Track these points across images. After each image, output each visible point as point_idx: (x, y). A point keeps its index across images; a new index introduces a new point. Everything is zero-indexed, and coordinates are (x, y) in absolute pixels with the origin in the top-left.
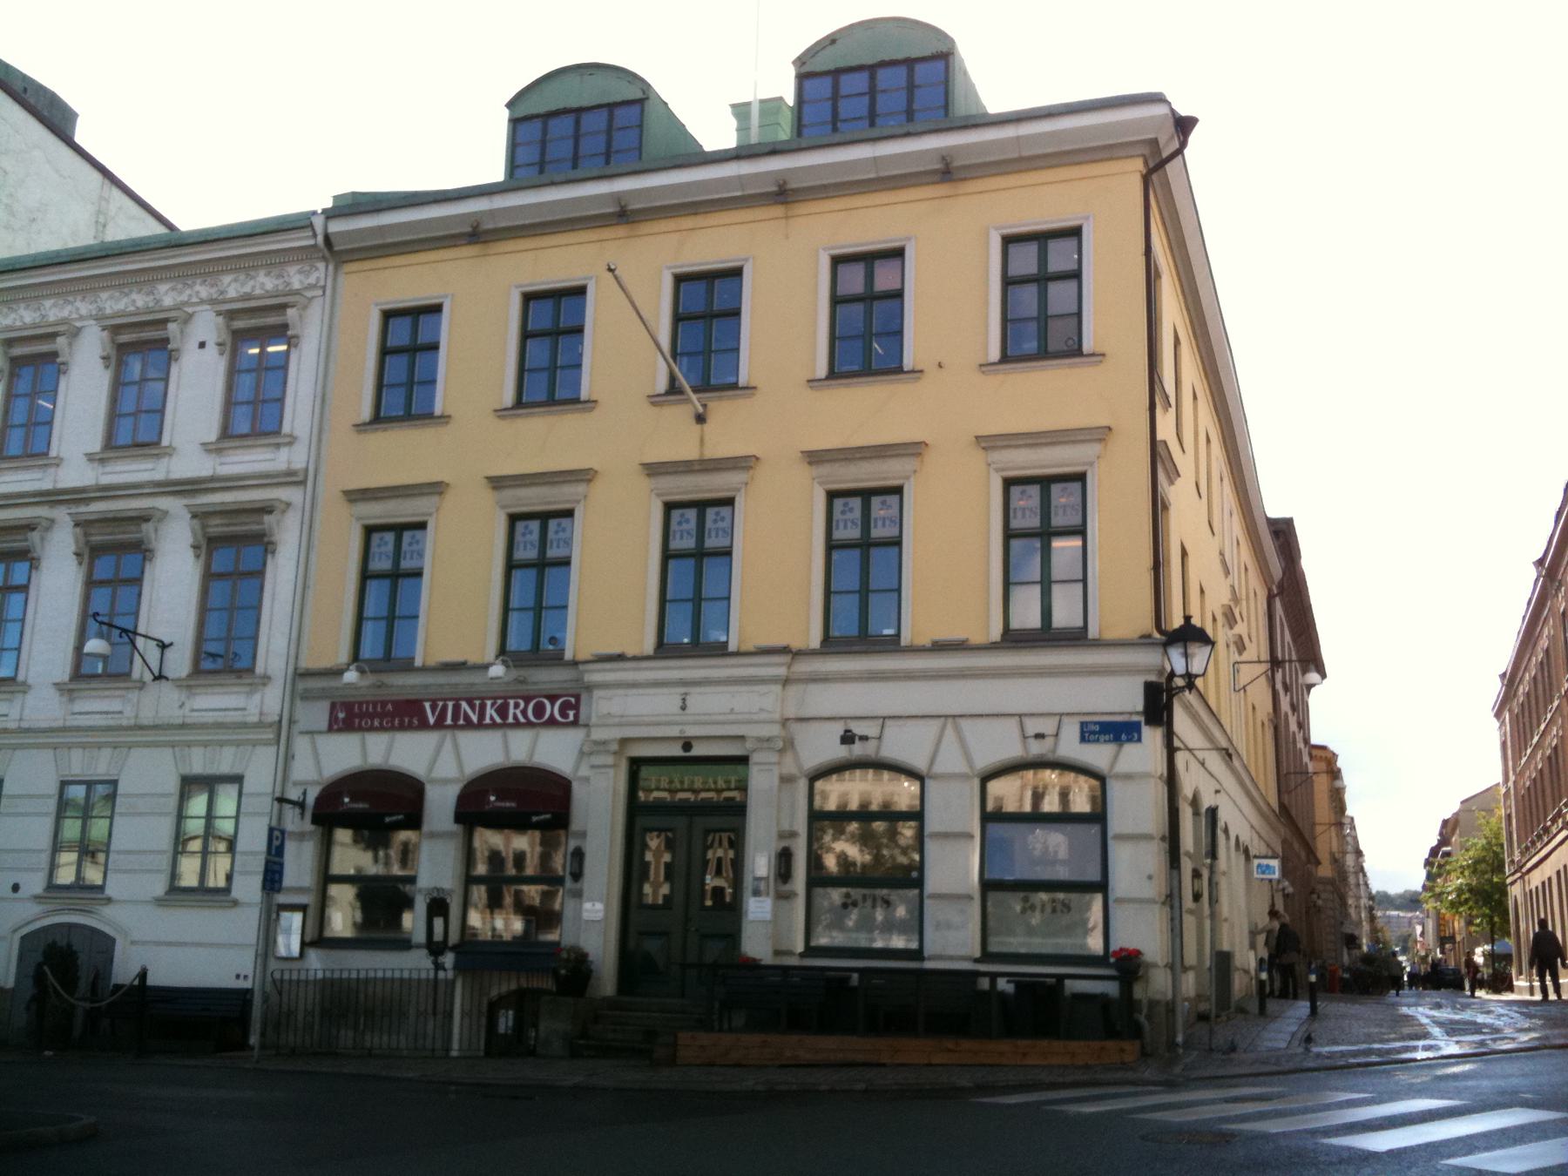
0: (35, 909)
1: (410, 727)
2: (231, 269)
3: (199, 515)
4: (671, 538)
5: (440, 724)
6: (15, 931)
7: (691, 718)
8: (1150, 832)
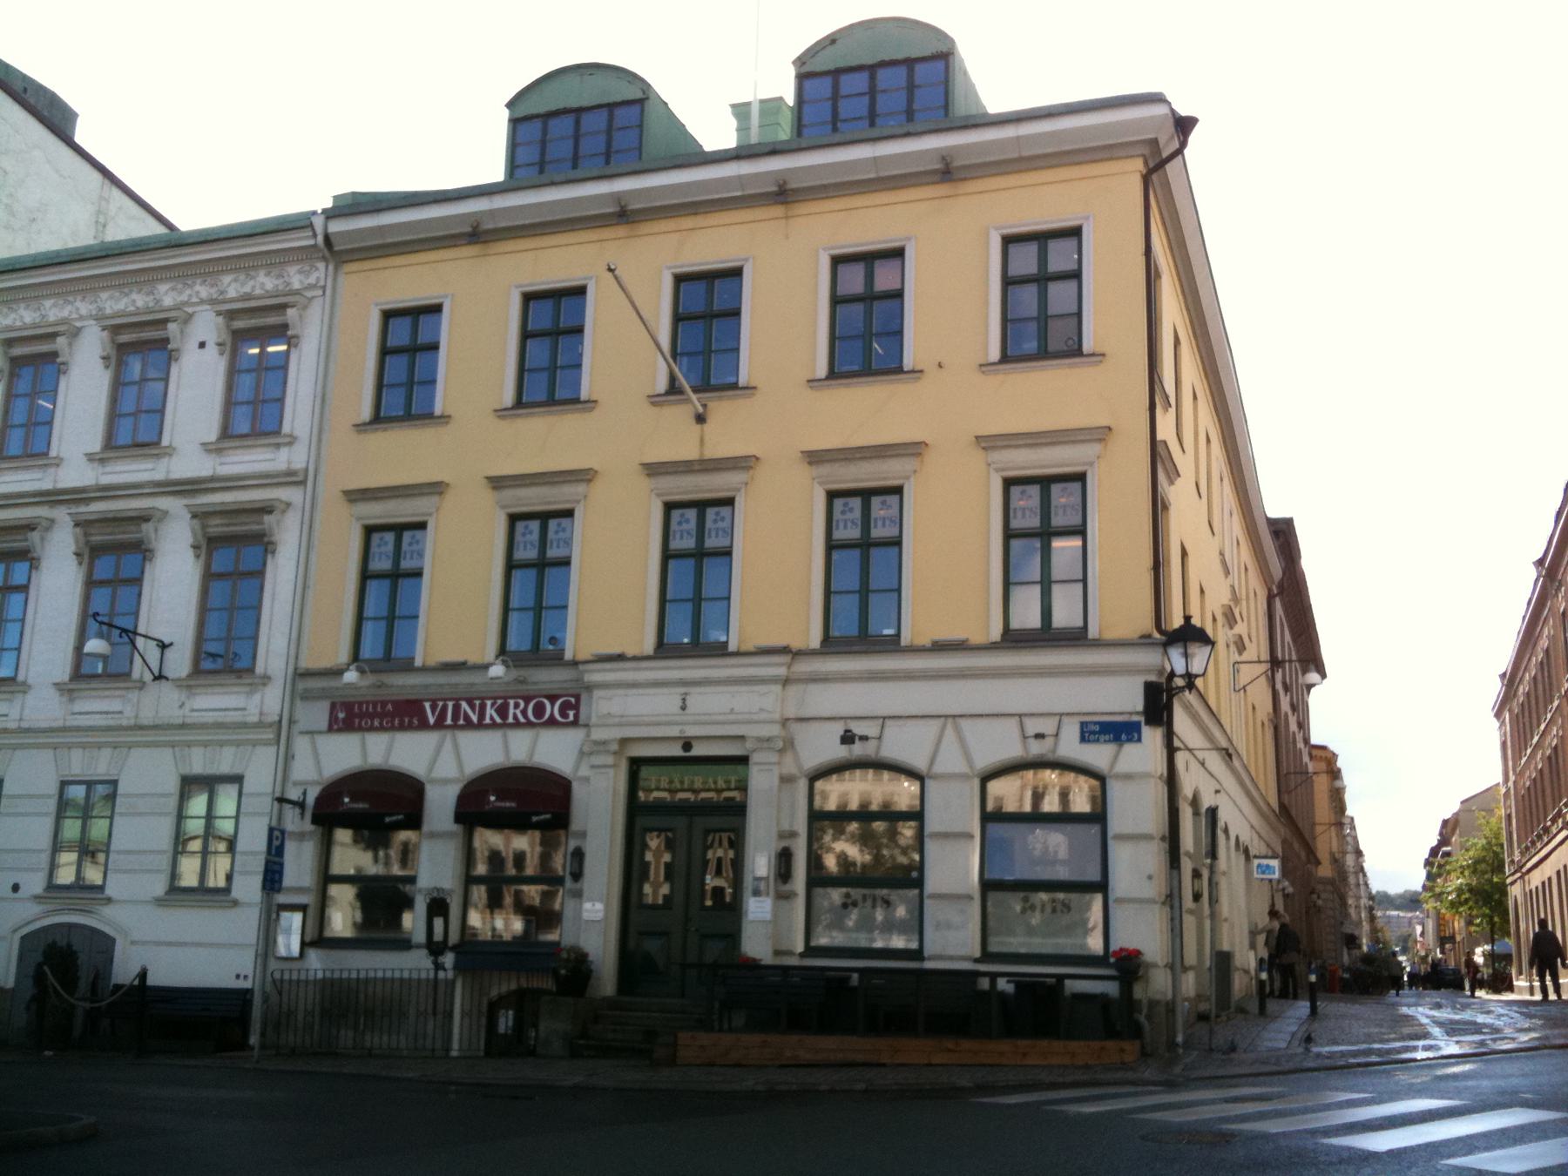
0: (35, 909)
1: (410, 727)
2: (231, 269)
3: (199, 515)
4: (671, 538)
5: (440, 724)
6: (15, 931)
7: (691, 718)
8: (1150, 832)
